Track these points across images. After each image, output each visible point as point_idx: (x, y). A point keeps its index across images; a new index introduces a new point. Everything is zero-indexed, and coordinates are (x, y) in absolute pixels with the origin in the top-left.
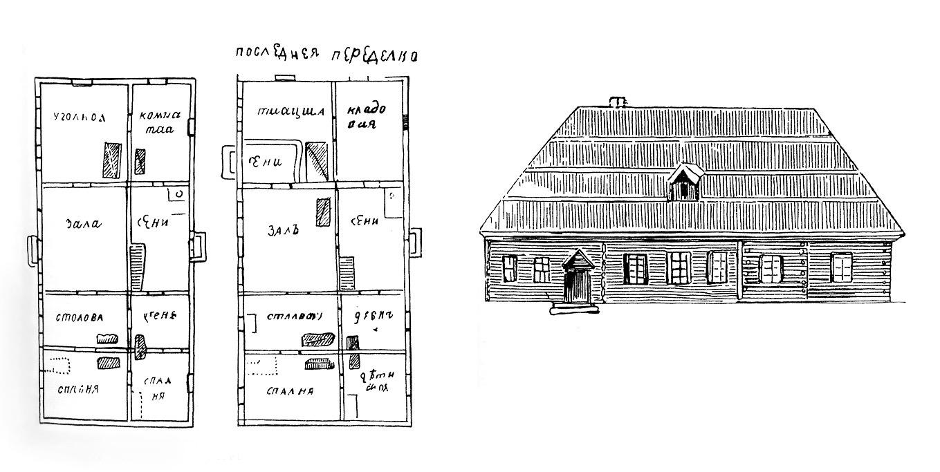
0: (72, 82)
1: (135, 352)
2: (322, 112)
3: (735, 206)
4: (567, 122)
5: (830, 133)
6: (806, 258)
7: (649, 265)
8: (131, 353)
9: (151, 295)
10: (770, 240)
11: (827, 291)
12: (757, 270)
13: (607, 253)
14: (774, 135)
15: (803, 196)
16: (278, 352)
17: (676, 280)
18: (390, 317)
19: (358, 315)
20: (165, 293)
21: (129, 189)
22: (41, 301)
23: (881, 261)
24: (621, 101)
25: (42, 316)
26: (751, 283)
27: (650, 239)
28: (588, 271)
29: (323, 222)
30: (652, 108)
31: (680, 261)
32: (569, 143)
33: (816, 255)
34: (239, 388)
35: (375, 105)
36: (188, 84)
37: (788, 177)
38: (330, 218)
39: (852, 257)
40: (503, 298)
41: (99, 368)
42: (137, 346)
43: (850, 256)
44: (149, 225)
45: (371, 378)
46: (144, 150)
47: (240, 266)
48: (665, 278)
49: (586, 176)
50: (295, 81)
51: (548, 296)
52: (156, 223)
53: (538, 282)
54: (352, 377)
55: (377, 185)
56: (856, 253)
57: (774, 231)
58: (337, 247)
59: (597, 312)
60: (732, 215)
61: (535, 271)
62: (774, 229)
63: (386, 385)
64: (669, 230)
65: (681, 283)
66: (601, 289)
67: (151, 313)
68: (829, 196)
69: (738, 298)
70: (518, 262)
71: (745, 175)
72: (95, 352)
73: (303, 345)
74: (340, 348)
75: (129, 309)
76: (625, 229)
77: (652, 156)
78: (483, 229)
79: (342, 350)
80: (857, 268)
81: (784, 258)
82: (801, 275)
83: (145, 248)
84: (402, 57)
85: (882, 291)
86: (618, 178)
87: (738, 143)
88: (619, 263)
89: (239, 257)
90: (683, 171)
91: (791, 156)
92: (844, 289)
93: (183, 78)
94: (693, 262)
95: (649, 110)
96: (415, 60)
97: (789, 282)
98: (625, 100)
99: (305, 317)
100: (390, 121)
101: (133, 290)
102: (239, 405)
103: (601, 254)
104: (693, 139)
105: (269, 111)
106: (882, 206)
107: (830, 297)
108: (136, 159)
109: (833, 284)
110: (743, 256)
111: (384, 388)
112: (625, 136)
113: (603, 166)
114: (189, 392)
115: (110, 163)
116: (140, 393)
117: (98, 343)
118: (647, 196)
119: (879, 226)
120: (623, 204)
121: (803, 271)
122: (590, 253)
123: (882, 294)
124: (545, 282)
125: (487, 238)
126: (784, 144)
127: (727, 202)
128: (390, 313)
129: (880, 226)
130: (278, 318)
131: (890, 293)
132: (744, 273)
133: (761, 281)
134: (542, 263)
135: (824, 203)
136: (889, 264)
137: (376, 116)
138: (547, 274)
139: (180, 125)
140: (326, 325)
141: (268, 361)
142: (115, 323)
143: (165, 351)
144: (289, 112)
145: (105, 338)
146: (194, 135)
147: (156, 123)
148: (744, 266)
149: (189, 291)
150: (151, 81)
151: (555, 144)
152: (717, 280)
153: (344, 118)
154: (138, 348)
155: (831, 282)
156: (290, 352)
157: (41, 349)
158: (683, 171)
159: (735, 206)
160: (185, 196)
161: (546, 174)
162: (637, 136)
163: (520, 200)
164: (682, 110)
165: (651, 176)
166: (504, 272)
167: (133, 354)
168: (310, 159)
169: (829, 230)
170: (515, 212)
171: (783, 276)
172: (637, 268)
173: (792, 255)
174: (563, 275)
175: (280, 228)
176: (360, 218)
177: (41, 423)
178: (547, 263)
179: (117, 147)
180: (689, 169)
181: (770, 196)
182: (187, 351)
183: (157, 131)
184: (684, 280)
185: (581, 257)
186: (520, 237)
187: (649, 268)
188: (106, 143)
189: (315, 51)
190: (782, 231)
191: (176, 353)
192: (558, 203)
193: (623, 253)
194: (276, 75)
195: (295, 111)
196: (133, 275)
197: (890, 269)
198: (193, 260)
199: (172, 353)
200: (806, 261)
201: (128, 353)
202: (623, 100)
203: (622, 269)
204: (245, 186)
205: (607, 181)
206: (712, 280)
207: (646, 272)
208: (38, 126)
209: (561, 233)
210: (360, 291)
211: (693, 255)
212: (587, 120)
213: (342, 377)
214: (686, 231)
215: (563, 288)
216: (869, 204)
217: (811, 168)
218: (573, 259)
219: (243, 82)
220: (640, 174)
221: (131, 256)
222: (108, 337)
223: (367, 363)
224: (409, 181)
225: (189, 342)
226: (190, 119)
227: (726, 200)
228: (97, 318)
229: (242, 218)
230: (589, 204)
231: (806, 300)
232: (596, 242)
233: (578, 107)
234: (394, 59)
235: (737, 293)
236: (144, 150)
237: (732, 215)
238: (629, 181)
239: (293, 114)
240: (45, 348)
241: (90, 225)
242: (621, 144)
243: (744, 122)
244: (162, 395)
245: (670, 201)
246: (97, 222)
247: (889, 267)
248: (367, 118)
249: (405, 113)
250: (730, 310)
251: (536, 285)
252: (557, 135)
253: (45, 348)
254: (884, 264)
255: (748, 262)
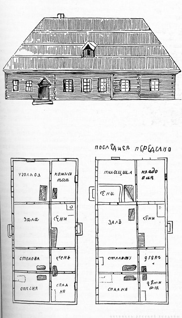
0: (26, 160)
1: (52, 273)
2: (131, 172)
3: (110, 59)
4: (39, 24)
5: (150, 28)
6: (139, 81)
7: (74, 84)
8: (51, 273)
9: (60, 249)
10: (124, 74)
11: (148, 95)
12: (119, 86)
13: (56, 79)
14: (126, 29)
15: (138, 55)
16: (113, 273)
17: (85, 90)
18: (159, 258)
19: (146, 257)
20: (66, 248)
21: (50, 205)
22: (13, 252)
23: (171, 82)
24: (62, 15)
25: (14, 258)
26: (116, 91)
27: (74, 73)
28: (48, 86)
29: (131, 219)
30: (75, 18)
31: (87, 82)
32: (40, 33)
33: (144, 80)
34: (96, 288)
35: (153, 170)
36: (75, 161)
37: (132, 47)
38: (134, 217)
39: (159, 81)
40: (13, 98)
41: (37, 280)
42: (53, 271)
43: (158, 80)
44: (59, 220)
45: (152, 284)
46: (57, 189)
47: (97, 237)
48: (80, 89)
49: (48, 47)
50: (119, 159)
51: (32, 97)
52: (61, 219)
53: (27, 91)
54: (144, 283)
55: (154, 203)
56: (160, 79)
57: (126, 70)
58: (137, 229)
59: (52, 104)
60: (109, 63)
61: (26, 86)
62: (126, 69)
63: (158, 287)
64: (82, 69)
65: (87, 92)
66: (54, 94)
67: (59, 257)
68: (149, 55)
69: (111, 98)
70: (19, 83)
71: (114, 46)
72: (36, 273)
73: (123, 270)
74: (139, 271)
75: (50, 255)
76: (64, 69)
77: (75, 38)
78: (4, 69)
79: (139, 272)
80: (161, 85)
81: (131, 81)
82: (137, 88)
83: (57, 229)
84: (165, 149)
85: (171, 95)
86: (61, 48)
87: (111, 33)
88: (61, 83)
89: (96, 233)
90: (88, 45)
91: (133, 38)
92: (156, 94)
93: (73, 159)
94: (92, 83)
95: (74, 19)
96: (170, 151)
97: (133, 91)
98: (64, 15)
99: (124, 258)
100: (159, 177)
101: (52, 247)
102: (96, 295)
103: (54, 79)
104: (92, 31)
105: (109, 172)
106: (171, 59)
107: (150, 97)
108: (53, 192)
109: (151, 92)
110: (113, 80)
111: (157, 288)
112: (64, 30)
113: (55, 43)
114: (75, 290)
115: (42, 194)
116: (55, 290)
117: (37, 269)
118: (73, 55)
119: (170, 68)
120: (63, 58)
121: (138, 87)
122: (49, 79)
123: (171, 96)
124: (30, 91)
125: (6, 73)
126: (130, 33)
127: (107, 58)
128: (159, 257)
129: (171, 67)
130: (112, 259)
131: (175, 96)
132: (113, 87)
133: (121, 91)
134: (29, 83)
135: (147, 58)
136: (174, 83)
137: (153, 174)
138: (31, 88)
139: (72, 178)
140: (133, 262)
141: (108, 277)
142: (44, 261)
143: (65, 272)
144: (118, 172)
145: (40, 267)
146: (77, 182)
147: (61, 177)
148: (114, 84)
149: (75, 247)
150: (60, 160)
151: (35, 33)
152: (102, 90)
153: (140, 175)
154: (54, 271)
155: (150, 91)
156: (117, 273)
157: (13, 272)
158: (88, 45)
159: (110, 59)
160: (74, 208)
161: (31, 46)
162: (69, 30)
163: (20, 57)
164: (88, 19)
165: (75, 47)
166: (13, 87)
167: (52, 274)
168: (126, 192)
169: (149, 69)
170: (18, 62)
171: (130, 89)
172: (69, 85)
173: (134, 80)
174: (38, 88)
175: (113, 221)
176: (147, 217)
177: (13, 303)
178: (31, 83)
179: (45, 187)
180: (91, 44)
181: (124, 55)
182: (75, 272)
183: (62, 181)
184: (88, 90)
185: (45, 81)
186: (20, 72)
187: (74, 85)
188: (40, 186)
189: (128, 147)
190: (129, 70)
191: (70, 273)
192: (36, 58)
193: (63, 79)
194: (111, 157)
195: (120, 172)
196: (52, 241)
197: (175, 86)
198: (77, 235)
199: (68, 273)
200: (139, 83)
201: (50, 273)
202: (63, 15)
203: (63, 85)
204: (99, 204)
205: (56, 49)
206: (100, 90)
207: (73, 87)
208: (12, 178)
209: (37, 71)
210: (147, 248)
211: (92, 80)
212: (48, 23)
213: (139, 283)
214: (89, 70)
215: (38, 94)
216: (166, 58)
217: (142, 44)
218: (42, 81)
219: (98, 160)
220: (70, 46)
221: (51, 233)
222: (41, 267)
223: (150, 277)
224: (167, 202)
225: (75, 269)
226: (76, 175)
227: (106, 57)
228: (37, 259)
229: (98, 217)
230: (49, 58)
231: (139, 99)
232: (52, 74)
233: (44, 18)
234: (161, 150)
235: (111, 96)
236: (57, 189)
237: (109, 63)
238: (65, 49)
239: (119, 173)
240: (15, 271)
241: (34, 220)
242: (62, 33)
243: (113, 24)
244: (64, 291)
245: (83, 57)
246: (37, 218)
247: (174, 85)
248: (150, 175)
249: (166, 173)
250: (107, 103)
251: (27, 92)
252: (35, 30)
253: (15, 271)
254: (172, 84)
255: (115, 83)
